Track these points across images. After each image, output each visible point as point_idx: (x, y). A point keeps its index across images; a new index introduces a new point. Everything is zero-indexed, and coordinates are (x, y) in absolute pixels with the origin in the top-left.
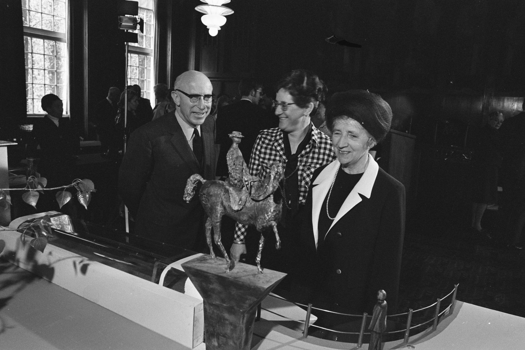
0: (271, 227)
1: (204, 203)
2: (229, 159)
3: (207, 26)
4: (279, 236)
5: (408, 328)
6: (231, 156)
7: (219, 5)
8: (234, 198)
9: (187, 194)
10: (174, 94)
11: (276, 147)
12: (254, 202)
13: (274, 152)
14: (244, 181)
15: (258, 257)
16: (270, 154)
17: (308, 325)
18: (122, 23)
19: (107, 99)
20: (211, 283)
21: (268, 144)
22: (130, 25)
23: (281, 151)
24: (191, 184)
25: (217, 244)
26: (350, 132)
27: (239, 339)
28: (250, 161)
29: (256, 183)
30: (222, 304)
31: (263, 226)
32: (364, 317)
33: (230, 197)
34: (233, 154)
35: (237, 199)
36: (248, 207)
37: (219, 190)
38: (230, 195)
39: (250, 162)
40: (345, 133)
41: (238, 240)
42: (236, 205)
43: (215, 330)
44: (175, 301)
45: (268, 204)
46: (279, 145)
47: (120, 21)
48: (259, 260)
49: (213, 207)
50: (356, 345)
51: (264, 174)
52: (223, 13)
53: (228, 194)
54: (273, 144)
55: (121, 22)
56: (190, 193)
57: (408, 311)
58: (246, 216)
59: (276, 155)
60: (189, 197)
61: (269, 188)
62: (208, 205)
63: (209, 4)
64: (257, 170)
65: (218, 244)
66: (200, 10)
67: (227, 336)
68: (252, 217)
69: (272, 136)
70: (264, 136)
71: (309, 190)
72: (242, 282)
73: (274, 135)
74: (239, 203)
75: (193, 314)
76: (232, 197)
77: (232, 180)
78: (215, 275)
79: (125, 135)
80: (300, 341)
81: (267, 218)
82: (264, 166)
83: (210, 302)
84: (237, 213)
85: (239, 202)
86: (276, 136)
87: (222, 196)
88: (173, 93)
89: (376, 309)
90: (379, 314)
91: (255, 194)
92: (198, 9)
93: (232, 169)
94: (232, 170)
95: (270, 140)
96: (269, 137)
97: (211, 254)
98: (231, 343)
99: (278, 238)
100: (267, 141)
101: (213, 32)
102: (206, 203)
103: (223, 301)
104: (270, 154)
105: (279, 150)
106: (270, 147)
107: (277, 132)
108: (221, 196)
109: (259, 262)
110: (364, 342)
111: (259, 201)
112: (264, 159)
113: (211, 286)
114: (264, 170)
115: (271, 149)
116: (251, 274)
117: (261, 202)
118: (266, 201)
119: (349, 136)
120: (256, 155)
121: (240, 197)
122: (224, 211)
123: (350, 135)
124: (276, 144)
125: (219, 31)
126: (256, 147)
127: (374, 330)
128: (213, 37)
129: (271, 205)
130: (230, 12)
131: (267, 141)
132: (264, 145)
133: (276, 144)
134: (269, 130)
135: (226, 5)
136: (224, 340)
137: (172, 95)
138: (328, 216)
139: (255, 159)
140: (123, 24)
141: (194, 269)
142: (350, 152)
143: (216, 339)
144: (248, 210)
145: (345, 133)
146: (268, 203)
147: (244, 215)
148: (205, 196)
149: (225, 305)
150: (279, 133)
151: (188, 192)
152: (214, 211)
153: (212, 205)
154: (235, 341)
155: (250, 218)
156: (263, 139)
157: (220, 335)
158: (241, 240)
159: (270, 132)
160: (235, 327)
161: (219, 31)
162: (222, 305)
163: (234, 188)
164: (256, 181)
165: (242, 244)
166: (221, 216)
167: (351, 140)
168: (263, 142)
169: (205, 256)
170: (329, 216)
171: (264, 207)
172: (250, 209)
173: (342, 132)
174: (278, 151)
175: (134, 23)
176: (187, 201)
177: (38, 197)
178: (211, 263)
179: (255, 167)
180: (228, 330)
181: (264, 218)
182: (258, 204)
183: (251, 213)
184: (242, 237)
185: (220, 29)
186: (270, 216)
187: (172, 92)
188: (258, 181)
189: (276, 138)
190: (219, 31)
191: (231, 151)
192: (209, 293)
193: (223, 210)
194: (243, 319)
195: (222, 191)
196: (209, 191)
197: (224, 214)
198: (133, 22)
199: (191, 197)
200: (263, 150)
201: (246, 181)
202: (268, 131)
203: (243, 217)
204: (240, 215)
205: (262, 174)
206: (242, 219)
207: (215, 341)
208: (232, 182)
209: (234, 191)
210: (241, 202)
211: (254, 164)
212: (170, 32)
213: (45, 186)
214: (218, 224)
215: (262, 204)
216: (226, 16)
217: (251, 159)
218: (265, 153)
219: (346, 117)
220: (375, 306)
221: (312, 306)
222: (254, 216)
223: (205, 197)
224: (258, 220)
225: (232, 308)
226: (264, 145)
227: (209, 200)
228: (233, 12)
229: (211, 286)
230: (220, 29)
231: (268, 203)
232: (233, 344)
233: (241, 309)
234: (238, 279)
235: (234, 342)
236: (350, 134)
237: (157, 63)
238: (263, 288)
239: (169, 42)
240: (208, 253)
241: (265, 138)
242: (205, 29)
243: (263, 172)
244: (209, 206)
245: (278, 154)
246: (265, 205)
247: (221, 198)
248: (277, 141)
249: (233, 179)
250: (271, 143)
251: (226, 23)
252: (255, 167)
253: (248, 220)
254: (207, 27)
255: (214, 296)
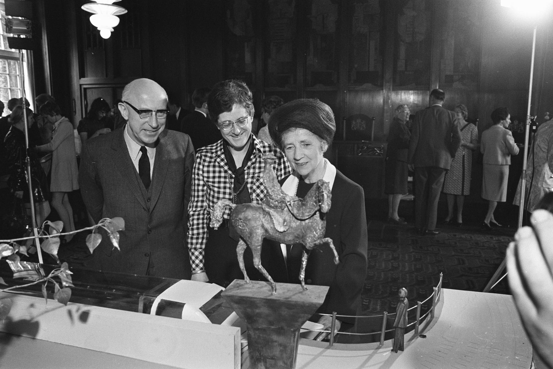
0: (327, 244)
1: (240, 227)
2: (267, 182)
3: (97, 28)
4: (337, 251)
5: (418, 319)
6: (269, 178)
7: (109, 4)
8: (278, 220)
9: (215, 221)
11: (219, 163)
12: (299, 221)
13: (217, 169)
14: (286, 202)
15: (302, 275)
16: (214, 172)
17: (334, 333)
18: (12, 27)
20: (257, 307)
21: (210, 162)
22: (22, 30)
23: (225, 166)
24: (219, 210)
25: (257, 268)
26: (302, 142)
27: (290, 358)
28: (193, 183)
29: (296, 202)
30: (270, 327)
31: (315, 244)
32: (385, 316)
33: (273, 219)
34: (269, 176)
35: (281, 220)
36: (293, 227)
37: (257, 213)
38: (272, 217)
39: (193, 184)
40: (298, 145)
41: (197, 269)
42: (281, 227)
43: (262, 354)
44: (210, 333)
45: (316, 222)
46: (222, 160)
47: (11, 25)
48: (304, 277)
49: (253, 231)
50: (378, 343)
51: (212, 193)
52: (114, 13)
53: (269, 217)
54: (215, 160)
55: (11, 26)
56: (219, 219)
57: (417, 304)
58: (291, 236)
59: (220, 172)
60: (217, 224)
61: (325, 206)
62: (246, 229)
63: (98, 3)
64: (203, 191)
65: (259, 268)
66: (87, 9)
67: (276, 358)
68: (298, 236)
69: (212, 153)
70: (204, 154)
72: (296, 301)
73: (214, 151)
74: (285, 224)
75: (234, 342)
76: (275, 218)
77: (272, 202)
78: (264, 299)
79: (16, 164)
80: (329, 350)
81: (316, 235)
82: (210, 186)
83: (255, 327)
84: (281, 234)
85: (284, 223)
86: (216, 152)
87: (262, 219)
89: (400, 307)
90: (403, 311)
91: (298, 213)
92: (85, 7)
93: (272, 191)
94: (272, 193)
95: (211, 158)
96: (209, 155)
97: (245, 278)
98: (281, 363)
99: (336, 253)
100: (208, 159)
101: (106, 34)
102: (244, 228)
103: (271, 323)
104: (214, 172)
105: (223, 165)
106: (212, 164)
107: (217, 148)
108: (260, 219)
109: (303, 279)
110: (386, 339)
111: (305, 220)
112: (208, 177)
113: (257, 311)
114: (210, 189)
115: (214, 166)
116: (297, 292)
117: (307, 221)
118: (312, 219)
119: (302, 146)
120: (200, 175)
121: (283, 218)
122: (265, 234)
123: (303, 145)
124: (218, 160)
127: (399, 326)
128: (104, 39)
129: (318, 223)
130: (123, 11)
131: (208, 159)
132: (206, 164)
133: (218, 160)
134: (207, 147)
135: (115, 4)
136: (273, 362)
139: (199, 180)
140: (14, 27)
141: (236, 296)
142: (307, 162)
143: (262, 364)
144: (294, 230)
145: (298, 145)
146: (315, 221)
147: (289, 236)
148: (242, 221)
149: (273, 327)
150: (219, 149)
151: (217, 218)
152: (255, 235)
154: (285, 361)
155: (297, 237)
156: (203, 157)
157: (268, 358)
158: (201, 269)
159: (208, 149)
160: (285, 347)
161: (112, 32)
162: (270, 328)
163: (275, 210)
164: (296, 201)
165: (203, 272)
166: (262, 239)
167: (305, 150)
168: (204, 161)
169: (238, 282)
171: (312, 225)
172: (296, 229)
173: (295, 144)
174: (222, 167)
175: (28, 27)
176: (216, 228)
177: (58, 245)
178: (249, 288)
179: (200, 188)
180: (277, 352)
181: (314, 236)
182: (303, 223)
183: (298, 233)
184: (201, 265)
185: (113, 30)
186: (319, 234)
188: (298, 200)
189: (217, 153)
191: (267, 173)
192: (255, 318)
193: (263, 233)
194: (294, 337)
195: (260, 213)
196: (246, 215)
197: (264, 237)
198: (26, 26)
199: (220, 224)
200: (206, 169)
201: (288, 202)
202: (206, 148)
203: (288, 237)
204: (285, 236)
205: (210, 194)
206: (287, 240)
207: (261, 365)
208: (272, 204)
209: (275, 213)
210: (287, 223)
211: (198, 185)
212: (44, 34)
213: (61, 231)
214: (259, 247)
215: (309, 223)
216: (118, 16)
217: (193, 181)
218: (208, 172)
219: (293, 128)
220: (399, 303)
221: (337, 314)
222: (301, 235)
223: (241, 222)
224: (308, 239)
225: (282, 328)
226: (206, 164)
227: (247, 225)
228: (126, 11)
229: (257, 311)
230: (113, 30)
231: (315, 221)
232: (283, 365)
233: (291, 328)
234: (290, 299)
235: (284, 363)
236: (302, 143)
237: (32, 72)
238: (319, 304)
239: (45, 45)
240: (243, 278)
241: (206, 156)
242: (95, 31)
243: (210, 192)
244: (248, 230)
245: (222, 170)
246: (313, 224)
247: (261, 221)
248: (219, 156)
249: (273, 201)
250: (213, 160)
252: (200, 188)
253: (293, 240)
254: (98, 29)
255: (260, 320)
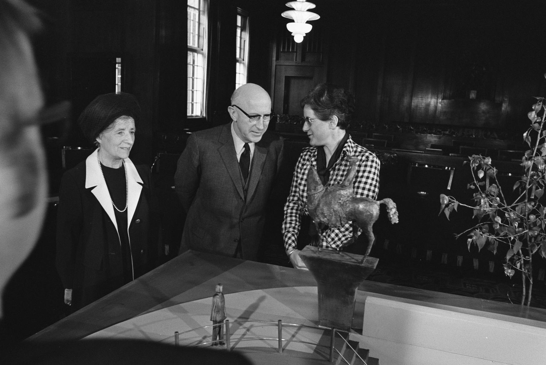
10: (231, 109)
19: (523, 136)
71: (473, 194)
88: (230, 108)
101: (299, 39)
125: (304, 37)
126: (297, 164)
137: (229, 110)
138: (119, 211)
153: (519, 218)
170: (120, 210)
185: (292, 34)
187: (230, 107)
190: (304, 37)
251: (311, 30)
